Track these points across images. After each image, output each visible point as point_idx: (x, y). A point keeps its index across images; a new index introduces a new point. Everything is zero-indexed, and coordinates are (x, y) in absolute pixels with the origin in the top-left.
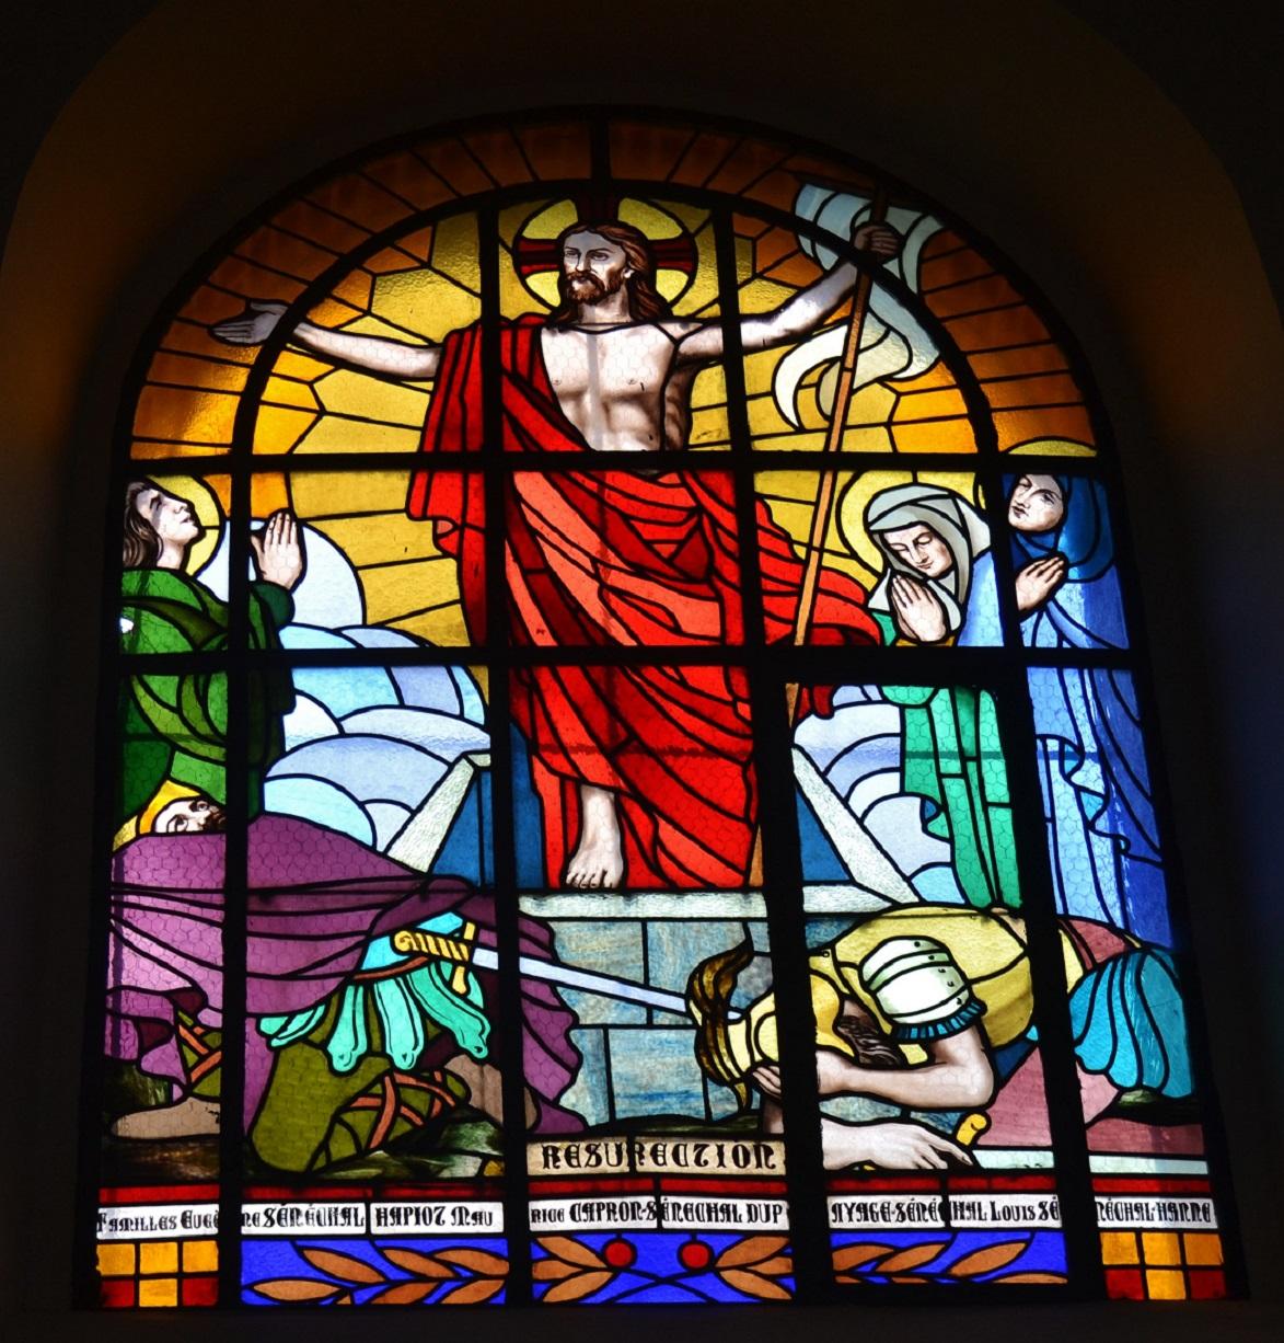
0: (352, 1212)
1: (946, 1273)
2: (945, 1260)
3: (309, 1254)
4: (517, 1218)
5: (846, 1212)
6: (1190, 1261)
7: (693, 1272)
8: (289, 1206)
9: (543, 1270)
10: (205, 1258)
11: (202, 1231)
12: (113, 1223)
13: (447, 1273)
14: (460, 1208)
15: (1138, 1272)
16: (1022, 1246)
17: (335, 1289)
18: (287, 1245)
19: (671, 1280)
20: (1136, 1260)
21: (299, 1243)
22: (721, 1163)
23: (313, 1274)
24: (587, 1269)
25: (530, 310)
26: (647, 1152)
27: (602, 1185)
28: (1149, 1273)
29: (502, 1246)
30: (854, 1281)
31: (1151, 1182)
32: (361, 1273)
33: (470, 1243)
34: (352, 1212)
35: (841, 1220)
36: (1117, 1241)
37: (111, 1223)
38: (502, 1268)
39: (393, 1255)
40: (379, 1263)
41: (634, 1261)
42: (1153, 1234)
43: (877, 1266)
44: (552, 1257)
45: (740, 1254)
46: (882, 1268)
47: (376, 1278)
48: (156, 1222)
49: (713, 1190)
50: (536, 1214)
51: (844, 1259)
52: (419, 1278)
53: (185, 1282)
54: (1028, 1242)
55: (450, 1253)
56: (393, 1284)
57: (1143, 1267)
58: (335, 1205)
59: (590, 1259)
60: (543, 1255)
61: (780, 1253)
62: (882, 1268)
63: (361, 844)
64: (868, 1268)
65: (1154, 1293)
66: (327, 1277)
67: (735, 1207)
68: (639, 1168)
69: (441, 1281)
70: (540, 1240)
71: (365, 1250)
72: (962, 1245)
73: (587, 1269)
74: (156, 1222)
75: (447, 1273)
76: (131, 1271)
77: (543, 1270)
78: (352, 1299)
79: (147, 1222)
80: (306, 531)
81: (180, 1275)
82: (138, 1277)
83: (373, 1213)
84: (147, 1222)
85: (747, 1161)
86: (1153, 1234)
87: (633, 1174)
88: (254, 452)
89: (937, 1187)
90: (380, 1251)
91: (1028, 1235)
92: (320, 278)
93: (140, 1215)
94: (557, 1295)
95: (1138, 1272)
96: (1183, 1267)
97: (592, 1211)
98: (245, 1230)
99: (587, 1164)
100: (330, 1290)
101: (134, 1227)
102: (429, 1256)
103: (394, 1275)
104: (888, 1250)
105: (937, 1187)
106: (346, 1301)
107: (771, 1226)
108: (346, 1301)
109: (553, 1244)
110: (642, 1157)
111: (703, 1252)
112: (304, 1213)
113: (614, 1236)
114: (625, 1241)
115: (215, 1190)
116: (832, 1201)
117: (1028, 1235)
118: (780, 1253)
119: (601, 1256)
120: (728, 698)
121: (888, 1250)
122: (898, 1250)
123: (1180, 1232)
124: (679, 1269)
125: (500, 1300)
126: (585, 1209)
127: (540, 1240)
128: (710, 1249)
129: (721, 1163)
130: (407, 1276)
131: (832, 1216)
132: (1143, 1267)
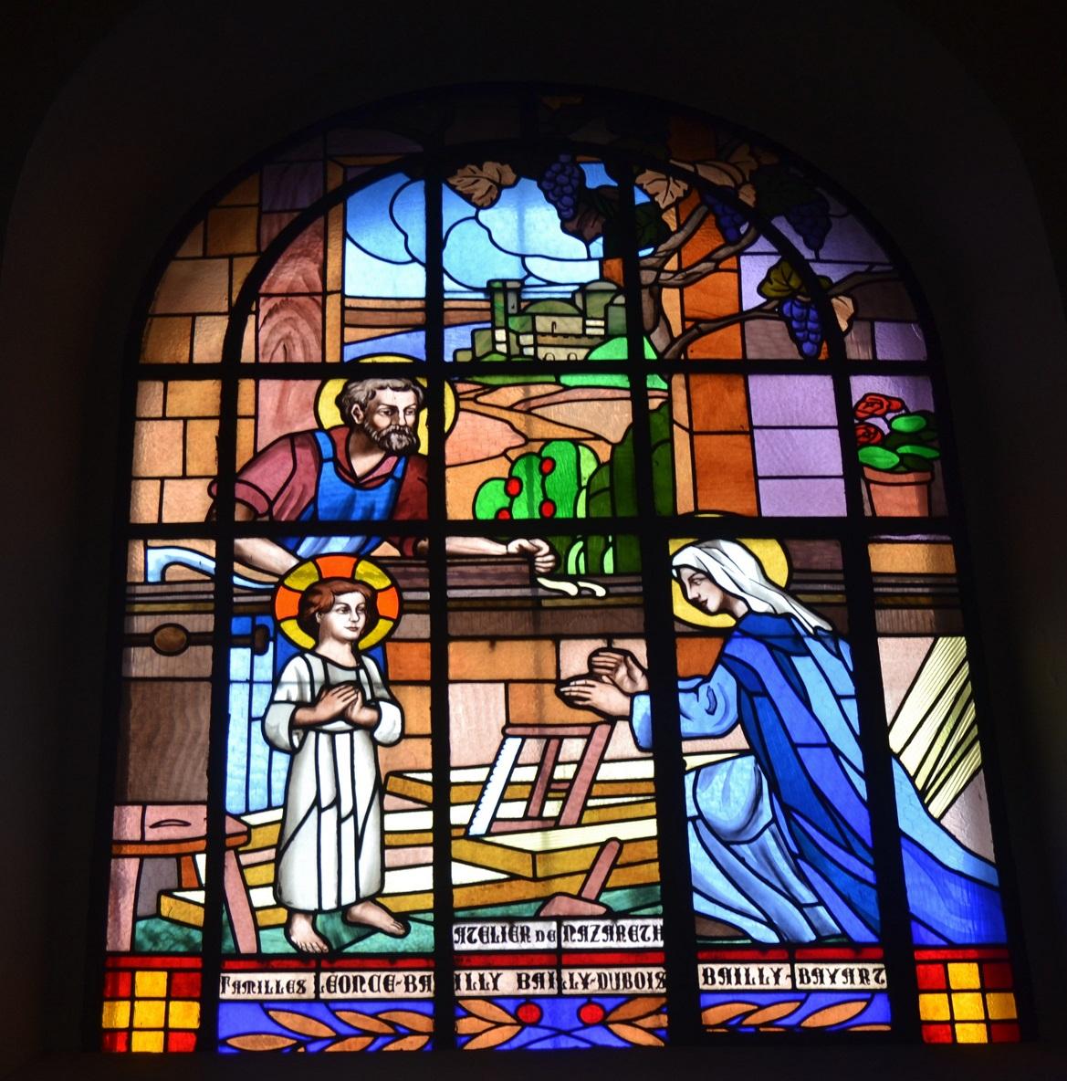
0: (733, 972)
4: (446, 984)
5: (713, 976)
7: (586, 1026)
12: (237, 985)
13: (387, 1029)
14: (249, 982)
15: (949, 1027)
16: (864, 1004)
17: (295, 1042)
18: (256, 1007)
19: (568, 1033)
20: (161, 1034)
21: (266, 1005)
23: (278, 1030)
24: (629, 1022)
25: (754, 246)
27: (491, 959)
28: (957, 1026)
29: (428, 1008)
30: (724, 1030)
32: (325, 1032)
34: (733, 972)
36: (553, 1022)
37: (234, 985)
38: (423, 1024)
40: (329, 1018)
42: (963, 1007)
43: (742, 1021)
44: (469, 1014)
45: (624, 1012)
47: (615, 1027)
49: (354, 966)
51: (714, 1016)
52: (364, 1033)
53: (944, 987)
54: (869, 1002)
56: (339, 1038)
57: (952, 1022)
59: (509, 1019)
60: (463, 1013)
63: (744, 729)
64: (734, 1022)
65: (961, 1039)
66: (286, 1032)
67: (747, 970)
69: (376, 1035)
70: (460, 1002)
71: (320, 1011)
72: (813, 1002)
73: (499, 1025)
75: (387, 1029)
77: (465, 1026)
78: (305, 1049)
80: (581, 448)
81: (166, 1029)
83: (323, 982)
85: (637, 975)
86: (963, 1007)
88: (846, 515)
89: (786, 956)
90: (333, 1012)
91: (868, 996)
94: (473, 1045)
97: (822, 976)
101: (256, 989)
102: (374, 1016)
103: (344, 1030)
106: (302, 1050)
108: (302, 1050)
109: (475, 1006)
110: (624, 935)
111: (600, 1009)
113: (522, 1001)
114: (534, 1004)
115: (879, 953)
117: (868, 996)
119: (514, 1016)
120: (584, 483)
122: (761, 1007)
125: (428, 1048)
127: (460, 1002)
128: (602, 1007)
131: (701, 979)
132: (952, 1022)
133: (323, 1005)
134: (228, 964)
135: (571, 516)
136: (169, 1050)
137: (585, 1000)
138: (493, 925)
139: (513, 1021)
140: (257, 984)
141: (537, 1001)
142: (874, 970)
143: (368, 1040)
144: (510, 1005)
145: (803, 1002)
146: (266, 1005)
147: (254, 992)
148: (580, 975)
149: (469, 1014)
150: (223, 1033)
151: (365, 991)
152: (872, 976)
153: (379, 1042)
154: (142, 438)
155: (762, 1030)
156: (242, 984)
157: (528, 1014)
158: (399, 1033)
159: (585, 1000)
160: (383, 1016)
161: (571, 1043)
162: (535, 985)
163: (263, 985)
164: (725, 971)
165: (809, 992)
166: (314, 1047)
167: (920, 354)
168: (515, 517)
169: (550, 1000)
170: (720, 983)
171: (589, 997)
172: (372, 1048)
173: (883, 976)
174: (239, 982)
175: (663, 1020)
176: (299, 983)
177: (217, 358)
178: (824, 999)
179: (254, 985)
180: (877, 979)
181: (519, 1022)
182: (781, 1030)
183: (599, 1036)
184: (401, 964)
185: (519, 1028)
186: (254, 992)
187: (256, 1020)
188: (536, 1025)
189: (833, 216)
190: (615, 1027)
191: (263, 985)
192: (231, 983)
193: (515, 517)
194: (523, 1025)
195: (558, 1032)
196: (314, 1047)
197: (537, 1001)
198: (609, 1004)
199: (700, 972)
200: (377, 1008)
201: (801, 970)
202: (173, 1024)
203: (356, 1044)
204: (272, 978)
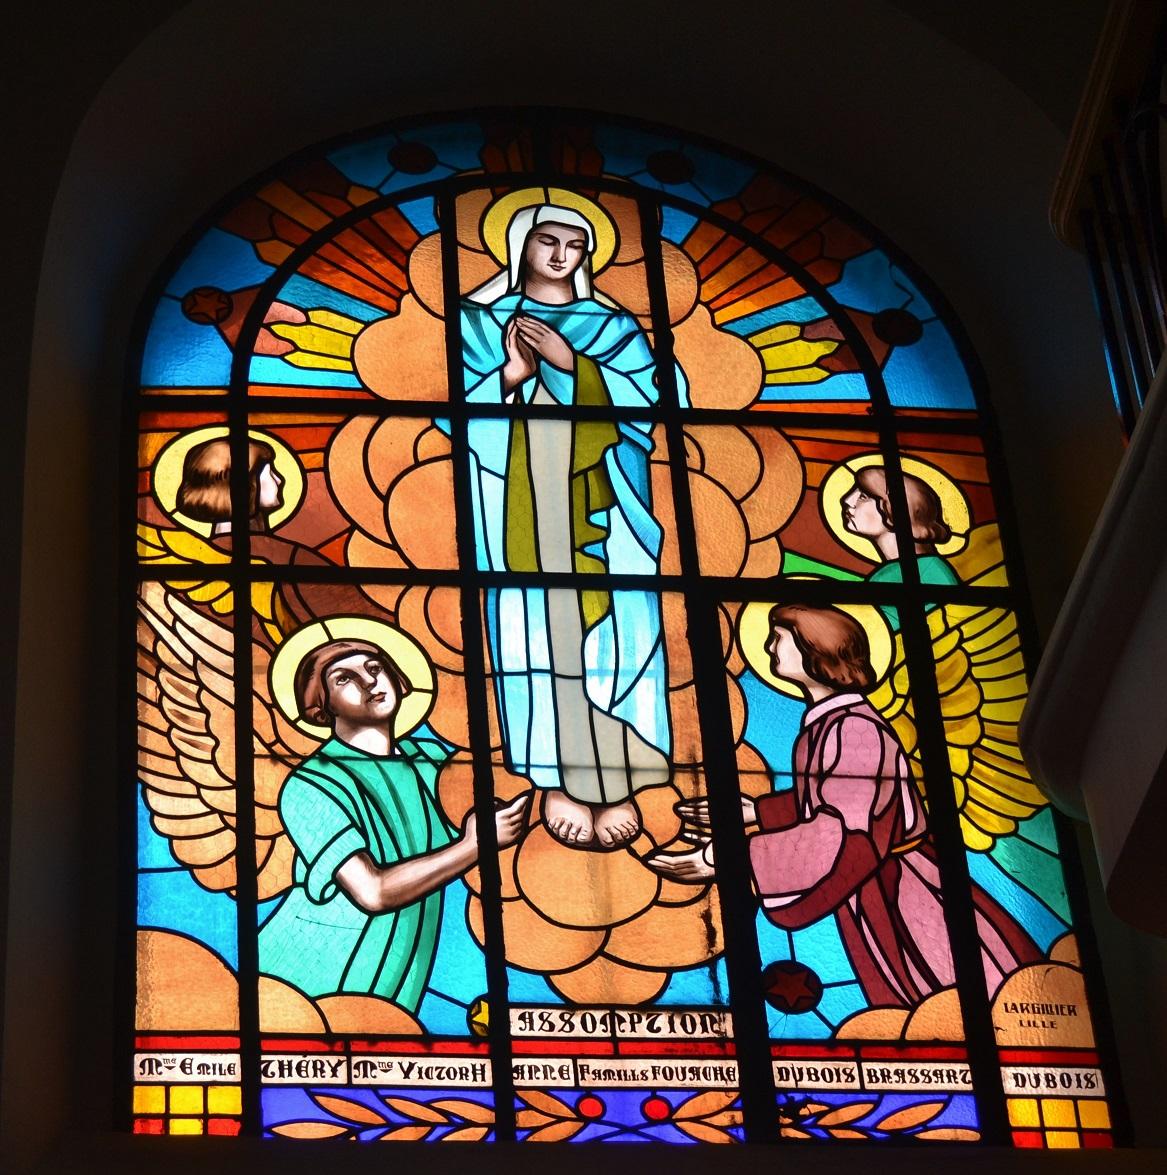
1: (874, 1128)
2: (874, 1118)
3: (320, 1099)
4: (504, 1073)
6: (1084, 1125)
7: (652, 1123)
8: (311, 1058)
9: (525, 1119)
10: (227, 1102)
11: (229, 1078)
13: (440, 1119)
15: (211, 1121)
20: (1036, 1123)
21: (312, 1090)
22: (672, 1030)
24: (697, 1120)
26: (285, 1018)
28: (1048, 1134)
31: (1033, 1054)
33: (457, 1094)
35: (523, 1078)
38: (487, 1116)
39: (394, 1102)
40: (378, 1106)
41: (604, 1113)
42: (1047, 1107)
44: (528, 1107)
46: (822, 1122)
47: (381, 1121)
48: (225, 1067)
50: (784, 1074)
52: (416, 1122)
53: (1086, 1135)
55: (863, 1112)
56: (392, 1127)
58: (290, 1058)
59: (566, 1112)
61: (729, 1108)
62: (822, 1122)
68: (619, 1034)
69: (434, 1126)
73: (560, 1119)
74: (225, 1067)
75: (440, 1119)
76: (161, 1109)
79: (629, 1073)
82: (1079, 1130)
84: (629, 1073)
85: (694, 1029)
86: (1047, 1107)
87: (614, 1040)
90: (382, 1099)
92: (286, 262)
93: (782, 1082)
95: (1039, 1134)
96: (1079, 1130)
97: (942, 1077)
98: (264, 1080)
99: (541, 1028)
100: (343, 1130)
101: (211, 1071)
102: (427, 1104)
104: (824, 1108)
105: (852, 1054)
106: (353, 1138)
107: (479, 1083)
108: (353, 1138)
109: (531, 1097)
112: (556, 1069)
116: (777, 1064)
117: (875, 1097)
118: (729, 1108)
119: (575, 1110)
121: (824, 1108)
122: (833, 1108)
123: (1075, 1099)
124: (643, 1121)
126: (896, 1072)
128: (667, 1102)
129: (672, 1030)
130: (406, 1121)
133: (371, 1092)
134: (265, 1045)
135: (258, 833)
136: (210, 1133)
137: (649, 1094)
138: (530, 1011)
139: (574, 1116)
140: (212, 1067)
141: (599, 1094)
142: (961, 1071)
143: (424, 1130)
144: (571, 1098)
145: (877, 1104)
146: (382, 1092)
147: (957, 1083)
148: (400, 1064)
149: (528, 1107)
150: (266, 1121)
151: (555, 1078)
152: (959, 1077)
153: (439, 1131)
154: (639, 469)
155: (835, 1132)
156: (687, 1070)
157: (589, 1107)
158: (458, 1123)
159: (649, 1094)
160: (436, 1105)
161: (635, 1138)
162: (692, 1076)
163: (217, 1067)
164: (527, 1016)
165: (882, 1093)
166: (367, 1136)
167: (965, 401)
168: (612, 572)
169: (618, 1094)
170: (691, 1079)
171: (653, 1090)
172: (431, 1138)
173: (969, 1077)
174: (599, 1071)
175: (739, 1116)
176: (647, 1078)
177: (445, 398)
178: (898, 1101)
179: (467, 1070)
180: (964, 1080)
181: (580, 1117)
182: (883, 1135)
183: (670, 1134)
184: (382, 1046)
185: (582, 1124)
186: (957, 1083)
187: (302, 1104)
188: (598, 1120)
189: (807, 264)
190: (381, 1121)
191: (217, 1067)
192: (591, 1071)
193: (612, 572)
194: (587, 1121)
195: (624, 1129)
196: (367, 1136)
197: (599, 1094)
198: (674, 1099)
199: (775, 1071)
200: (429, 1096)
201: (869, 1071)
202: (213, 1109)
203: (408, 1134)
204: (629, 1065)
